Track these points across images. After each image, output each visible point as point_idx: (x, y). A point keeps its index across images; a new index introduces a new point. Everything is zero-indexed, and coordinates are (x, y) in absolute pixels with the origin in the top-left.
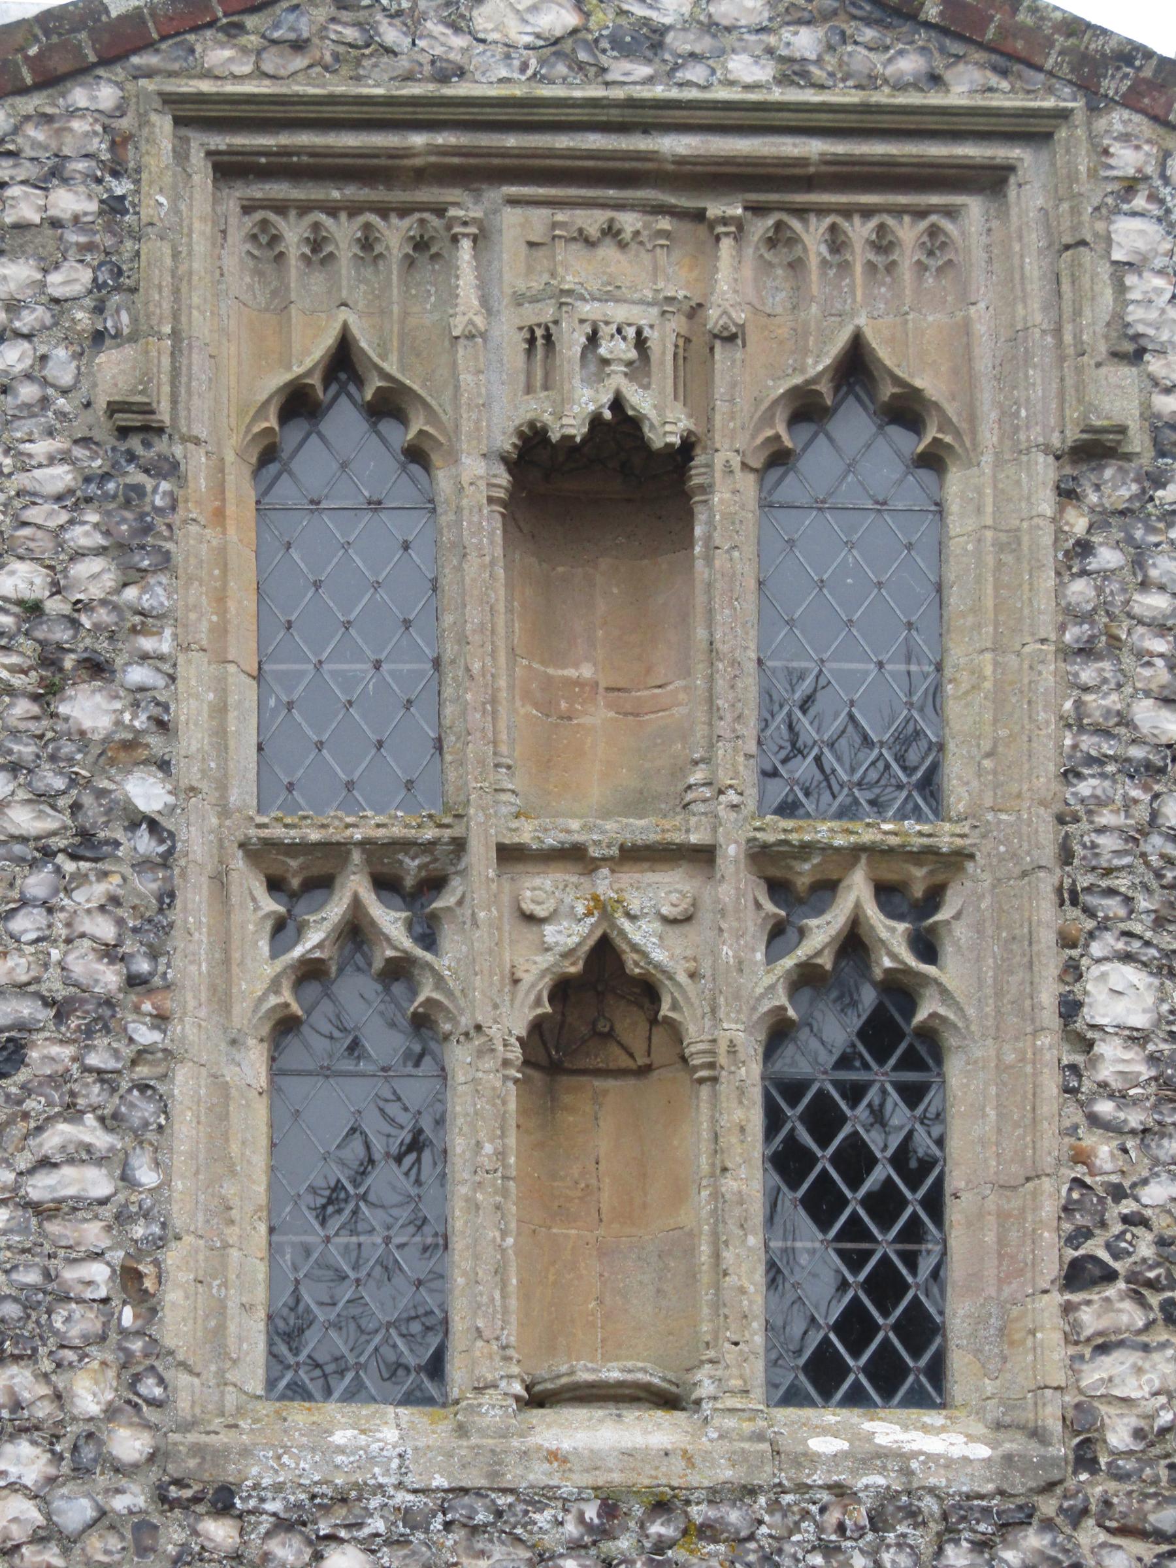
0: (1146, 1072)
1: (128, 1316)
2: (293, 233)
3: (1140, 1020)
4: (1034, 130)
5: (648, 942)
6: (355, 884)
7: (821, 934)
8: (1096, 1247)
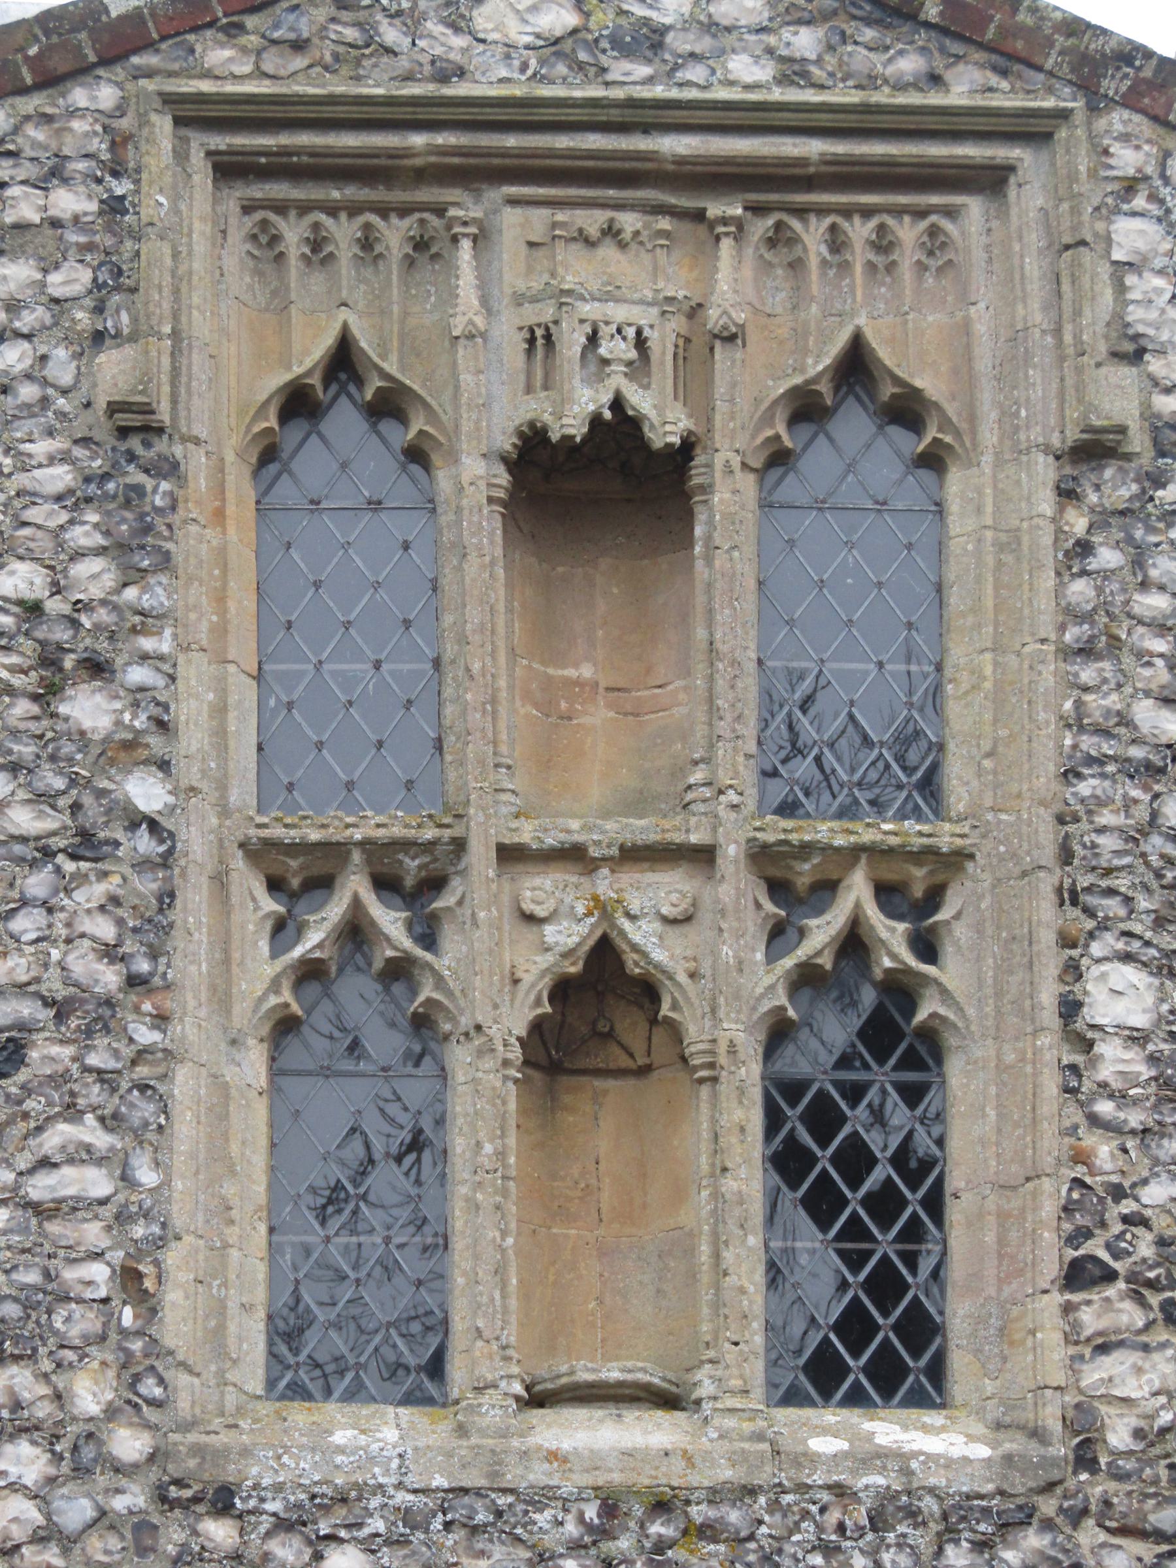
0: (1146, 1072)
1: (128, 1316)
2: (293, 233)
3: (1140, 1020)
4: (1034, 130)
5: (648, 942)
6: (355, 884)
7: (821, 934)
8: (1096, 1247)
